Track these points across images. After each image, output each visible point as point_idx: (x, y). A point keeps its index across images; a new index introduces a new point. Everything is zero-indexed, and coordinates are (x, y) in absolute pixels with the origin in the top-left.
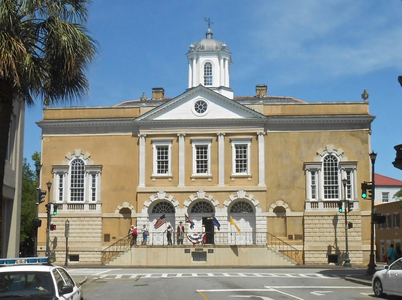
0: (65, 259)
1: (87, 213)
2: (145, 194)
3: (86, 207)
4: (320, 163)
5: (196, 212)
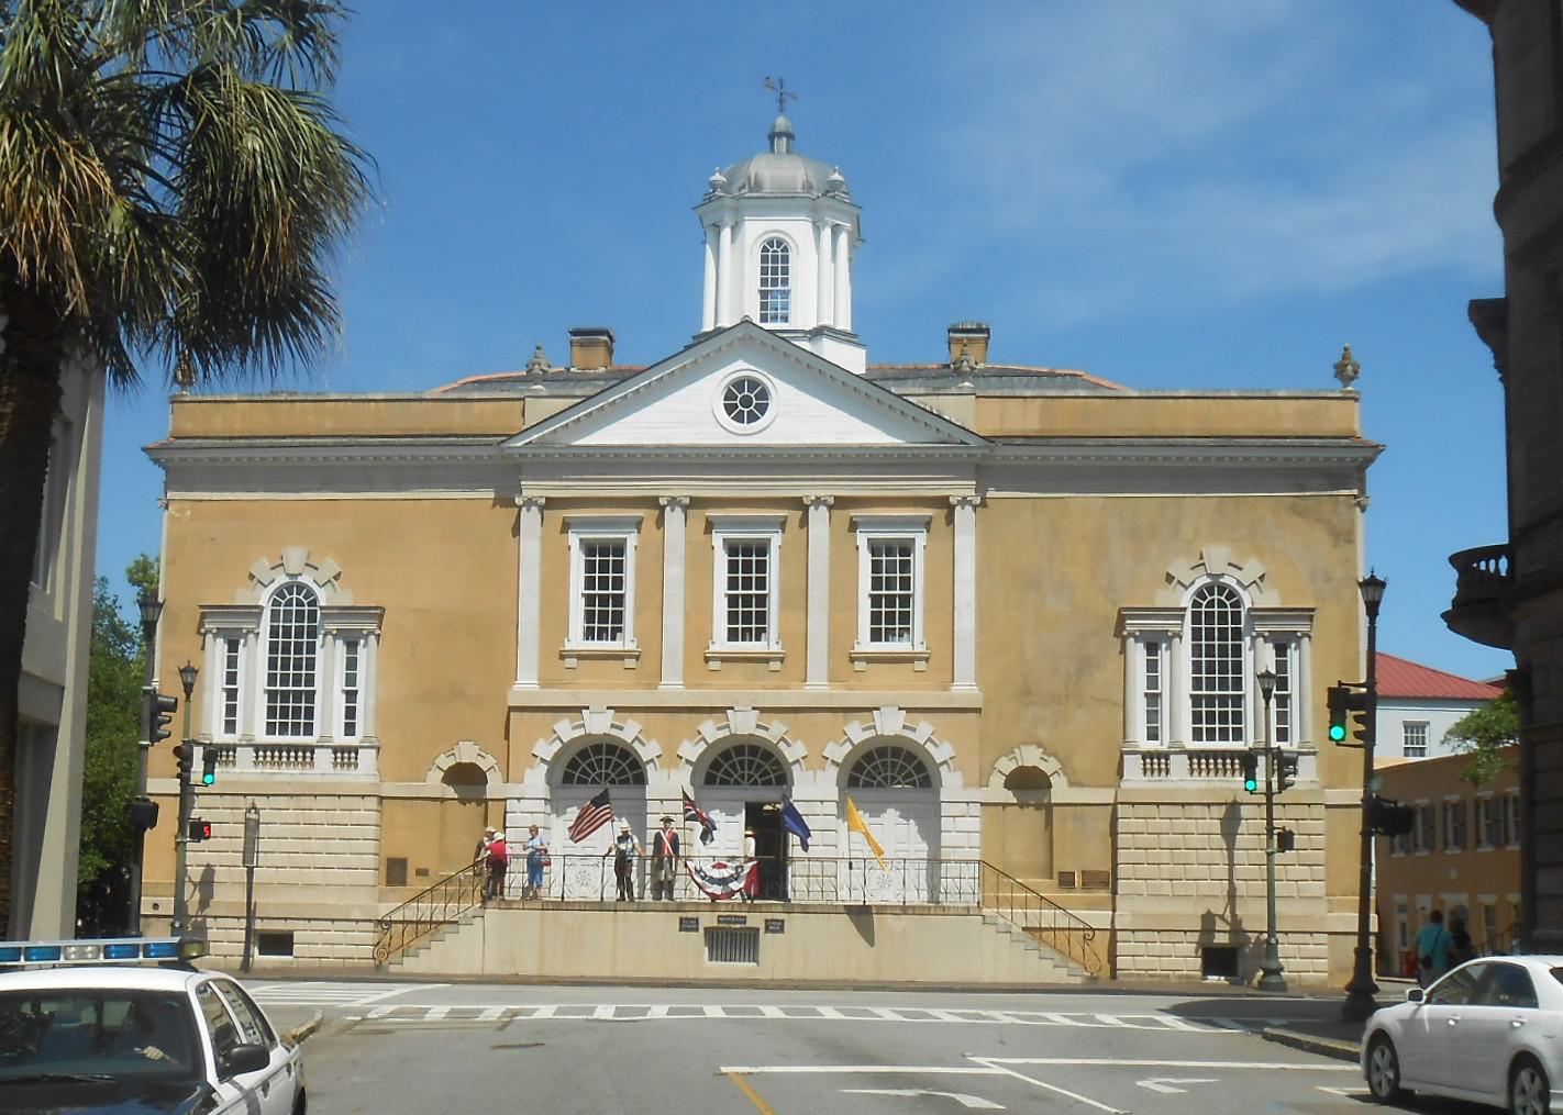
1: (327, 779)
3: (323, 758)
4: (1178, 613)
5: (723, 782)
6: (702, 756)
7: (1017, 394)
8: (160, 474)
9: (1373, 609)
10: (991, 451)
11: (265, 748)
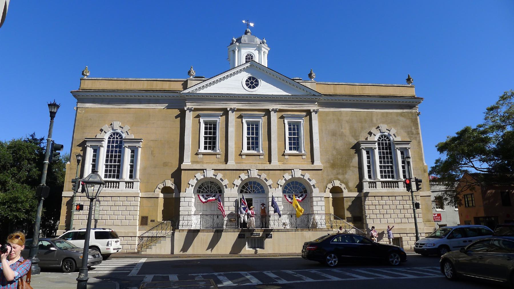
1: (123, 192)
2: (186, 171)
3: (122, 185)
4: (374, 142)
7: (327, 83)
8: (76, 100)
9: (53, 115)
11: (128, 182)
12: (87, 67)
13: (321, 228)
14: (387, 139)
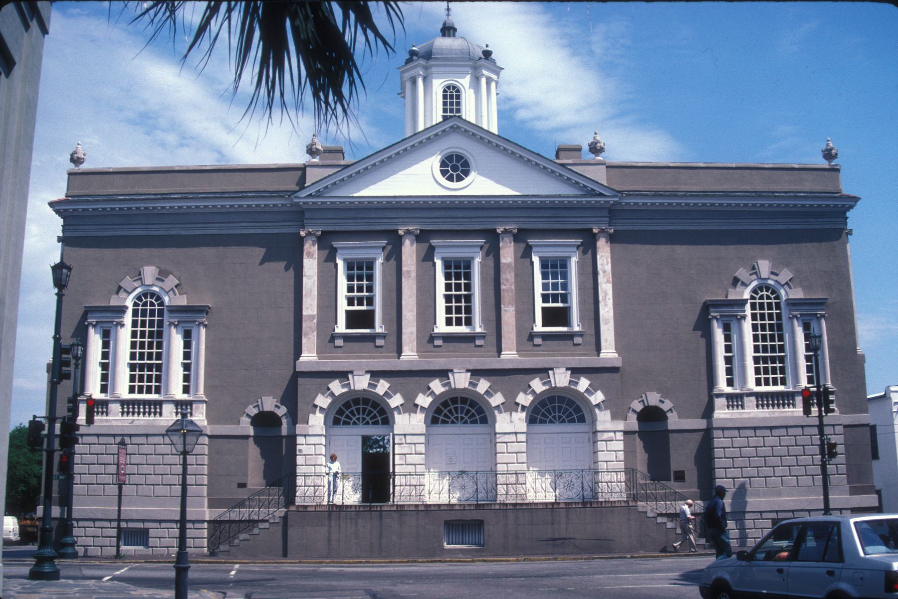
0: (115, 548)
5: (444, 422)
6: (532, 402)
10: (620, 199)
12: (829, 138)
13: (611, 500)
14: (772, 294)
